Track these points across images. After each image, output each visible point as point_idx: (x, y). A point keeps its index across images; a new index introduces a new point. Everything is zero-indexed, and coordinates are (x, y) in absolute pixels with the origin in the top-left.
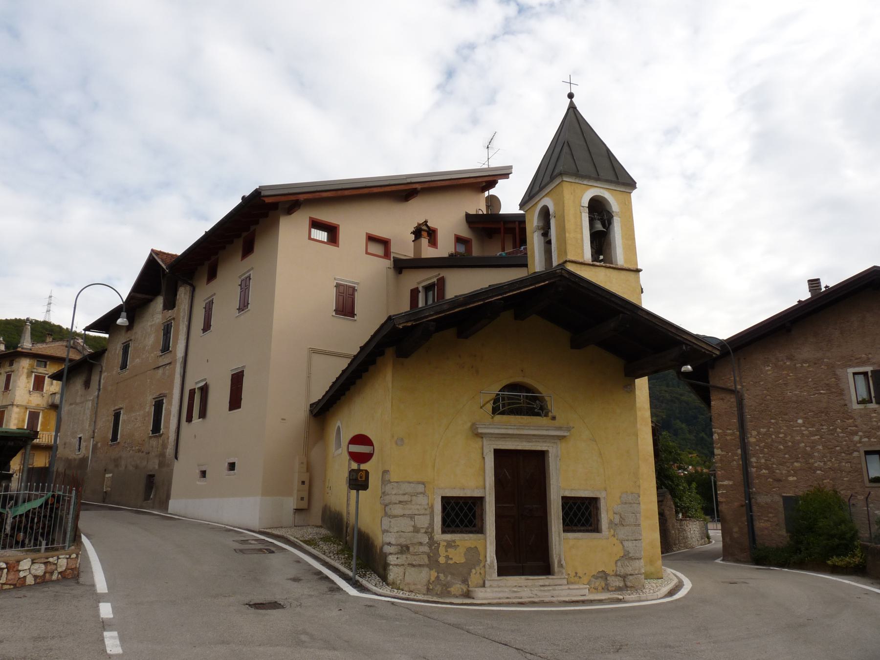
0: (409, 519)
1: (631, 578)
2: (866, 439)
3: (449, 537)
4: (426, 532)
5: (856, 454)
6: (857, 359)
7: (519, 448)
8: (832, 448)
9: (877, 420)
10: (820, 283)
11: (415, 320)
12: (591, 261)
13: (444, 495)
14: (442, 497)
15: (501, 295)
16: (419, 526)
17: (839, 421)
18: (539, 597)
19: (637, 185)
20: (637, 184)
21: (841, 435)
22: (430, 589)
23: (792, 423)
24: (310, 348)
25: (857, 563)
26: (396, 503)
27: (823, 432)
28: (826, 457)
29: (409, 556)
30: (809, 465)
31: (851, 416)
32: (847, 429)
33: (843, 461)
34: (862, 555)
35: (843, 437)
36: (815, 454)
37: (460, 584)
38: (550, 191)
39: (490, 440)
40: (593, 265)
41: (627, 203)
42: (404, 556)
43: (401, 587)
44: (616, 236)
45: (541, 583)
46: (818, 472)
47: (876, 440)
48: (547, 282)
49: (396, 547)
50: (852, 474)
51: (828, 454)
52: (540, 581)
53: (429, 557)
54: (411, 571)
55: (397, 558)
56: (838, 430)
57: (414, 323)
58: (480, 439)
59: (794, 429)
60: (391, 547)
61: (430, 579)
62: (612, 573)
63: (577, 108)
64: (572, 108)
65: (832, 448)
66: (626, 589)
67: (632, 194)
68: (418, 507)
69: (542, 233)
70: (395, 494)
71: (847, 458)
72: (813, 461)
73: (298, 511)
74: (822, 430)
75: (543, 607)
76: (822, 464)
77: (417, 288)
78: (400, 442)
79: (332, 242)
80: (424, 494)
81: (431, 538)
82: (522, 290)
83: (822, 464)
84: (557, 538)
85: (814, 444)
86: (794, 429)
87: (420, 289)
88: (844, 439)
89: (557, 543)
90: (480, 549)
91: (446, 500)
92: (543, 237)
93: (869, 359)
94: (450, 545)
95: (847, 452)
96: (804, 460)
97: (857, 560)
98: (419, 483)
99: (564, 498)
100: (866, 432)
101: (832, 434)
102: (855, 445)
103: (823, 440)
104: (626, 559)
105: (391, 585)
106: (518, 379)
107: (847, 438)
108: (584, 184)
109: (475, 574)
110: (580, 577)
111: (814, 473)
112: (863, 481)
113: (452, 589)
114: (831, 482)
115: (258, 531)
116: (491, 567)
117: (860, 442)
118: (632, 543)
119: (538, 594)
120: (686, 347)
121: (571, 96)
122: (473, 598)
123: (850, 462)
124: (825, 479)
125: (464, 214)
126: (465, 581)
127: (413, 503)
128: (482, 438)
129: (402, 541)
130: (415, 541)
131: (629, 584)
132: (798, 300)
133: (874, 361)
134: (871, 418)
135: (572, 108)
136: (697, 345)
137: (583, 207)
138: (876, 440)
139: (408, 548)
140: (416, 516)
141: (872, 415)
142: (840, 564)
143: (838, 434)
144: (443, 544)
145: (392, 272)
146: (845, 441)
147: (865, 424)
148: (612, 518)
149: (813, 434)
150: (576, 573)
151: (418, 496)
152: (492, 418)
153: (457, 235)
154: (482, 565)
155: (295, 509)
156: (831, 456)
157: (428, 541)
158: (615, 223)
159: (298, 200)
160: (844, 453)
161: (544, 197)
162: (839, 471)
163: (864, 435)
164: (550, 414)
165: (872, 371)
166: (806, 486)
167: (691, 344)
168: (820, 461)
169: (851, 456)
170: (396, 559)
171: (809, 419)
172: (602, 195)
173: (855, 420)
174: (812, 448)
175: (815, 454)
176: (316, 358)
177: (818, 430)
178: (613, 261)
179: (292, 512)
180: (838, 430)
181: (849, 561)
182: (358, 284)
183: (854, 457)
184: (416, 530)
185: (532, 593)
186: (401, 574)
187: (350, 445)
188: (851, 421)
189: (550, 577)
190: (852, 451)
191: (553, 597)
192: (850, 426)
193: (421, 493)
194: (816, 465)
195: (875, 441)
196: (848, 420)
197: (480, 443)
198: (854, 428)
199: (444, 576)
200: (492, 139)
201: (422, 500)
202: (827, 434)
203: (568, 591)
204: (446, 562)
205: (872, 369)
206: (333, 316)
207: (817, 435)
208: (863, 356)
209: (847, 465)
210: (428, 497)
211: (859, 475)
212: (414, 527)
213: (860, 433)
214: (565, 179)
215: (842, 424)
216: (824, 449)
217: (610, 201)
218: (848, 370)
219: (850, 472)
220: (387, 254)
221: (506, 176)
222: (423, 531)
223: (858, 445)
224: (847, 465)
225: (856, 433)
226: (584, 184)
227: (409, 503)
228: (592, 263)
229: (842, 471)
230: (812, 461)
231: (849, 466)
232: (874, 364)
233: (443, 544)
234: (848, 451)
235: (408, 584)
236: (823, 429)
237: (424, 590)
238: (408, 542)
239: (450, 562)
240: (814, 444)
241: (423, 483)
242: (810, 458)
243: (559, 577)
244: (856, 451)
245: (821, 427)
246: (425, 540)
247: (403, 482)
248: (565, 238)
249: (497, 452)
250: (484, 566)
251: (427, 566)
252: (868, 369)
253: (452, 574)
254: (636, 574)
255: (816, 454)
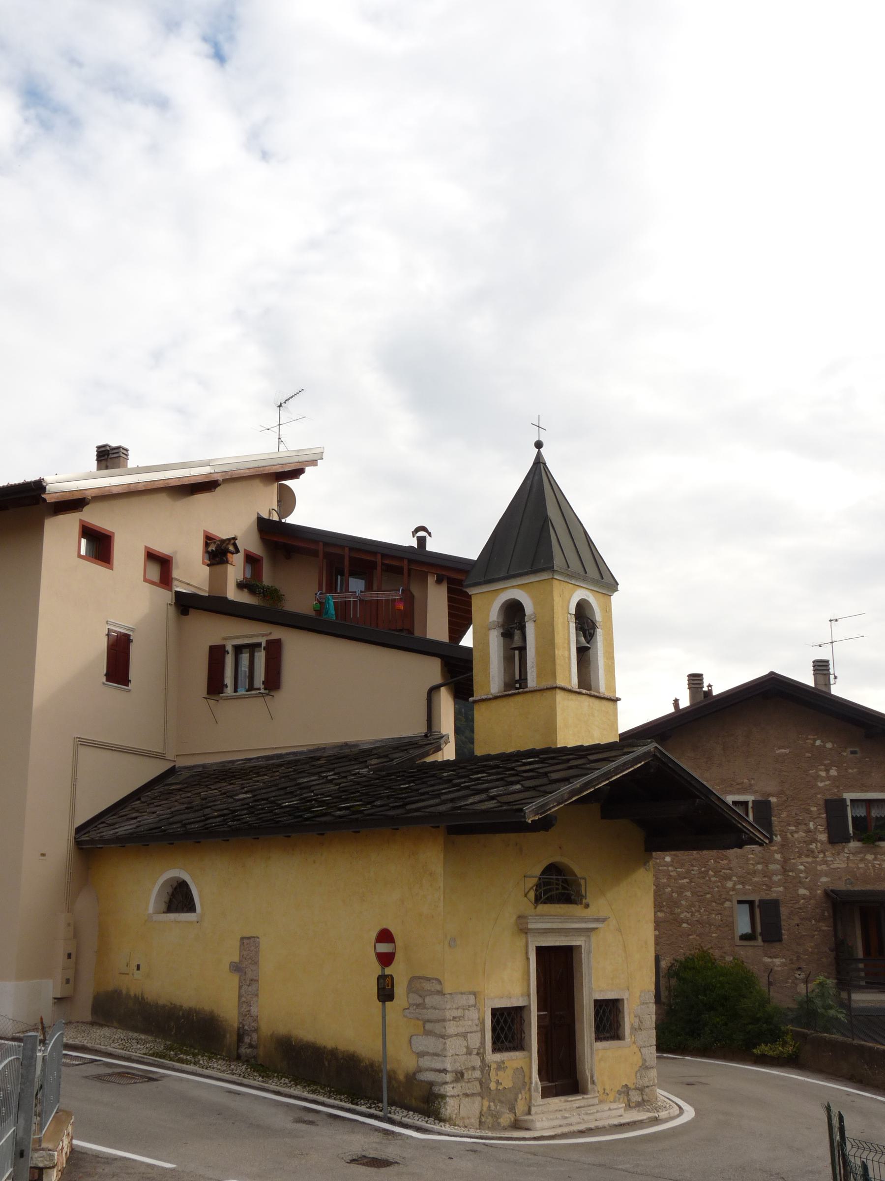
0: (463, 1039)
1: (647, 1090)
2: (739, 886)
3: (498, 1057)
4: (478, 1054)
5: (727, 904)
6: (738, 784)
7: (557, 944)
8: (702, 896)
9: (754, 862)
10: (702, 680)
11: (541, 814)
12: (577, 687)
13: (494, 1007)
14: (492, 1009)
15: (608, 779)
16: (471, 1047)
17: (712, 861)
18: (586, 1122)
19: (619, 587)
20: (619, 586)
21: (713, 879)
22: (483, 1122)
23: (658, 861)
24: (77, 738)
25: (790, 1052)
26: (450, 1020)
27: (693, 874)
28: (694, 906)
29: (463, 1084)
30: (674, 916)
31: (726, 856)
32: (721, 871)
33: (714, 912)
34: (795, 1043)
35: (715, 882)
36: (682, 902)
37: (508, 1114)
38: (527, 584)
39: (534, 936)
40: (580, 693)
41: (608, 610)
42: (459, 1085)
43: (457, 1123)
44: (599, 654)
45: (577, 1104)
46: (685, 925)
47: (750, 888)
48: (643, 763)
49: (451, 1074)
50: (721, 929)
51: (697, 903)
52: (577, 1102)
53: (481, 1084)
54: (465, 1101)
55: (453, 1088)
56: (711, 873)
57: (540, 817)
58: (523, 935)
59: (660, 868)
60: (446, 1074)
61: (482, 1110)
62: (633, 1087)
63: (547, 464)
64: (539, 464)
65: (702, 896)
66: (643, 1104)
67: (612, 597)
68: (470, 1023)
69: (502, 633)
70: (449, 1009)
71: (718, 908)
72: (679, 910)
73: (59, 1000)
74: (693, 872)
75: (612, 1134)
76: (689, 915)
77: (224, 646)
78: (452, 943)
79: (96, 558)
80: (475, 1007)
81: (483, 1061)
82: (624, 773)
83: (689, 915)
84: (589, 1050)
85: (682, 890)
86: (660, 868)
87: (229, 648)
88: (716, 884)
89: (589, 1057)
90: (526, 1070)
91: (495, 1012)
92: (502, 638)
93: (751, 785)
94: (500, 1066)
95: (718, 902)
96: (668, 910)
97: (789, 1049)
98: (470, 993)
99: (596, 1001)
100: (740, 877)
101: (704, 878)
102: (728, 893)
103: (693, 884)
104: (643, 1068)
105: (447, 1121)
106: (557, 859)
107: (719, 884)
108: (572, 584)
109: (521, 1099)
110: (608, 1094)
111: (678, 926)
112: (733, 938)
113: (501, 1120)
114: (698, 938)
115: (10, 1037)
116: (536, 1090)
117: (733, 889)
118: (649, 1050)
119: (585, 1118)
120: (745, 836)
121: (539, 445)
122: (528, 1129)
123: (721, 914)
124: (691, 935)
125: (255, 517)
126: (512, 1109)
127: (466, 1018)
128: (526, 933)
129: (458, 1067)
130: (470, 1065)
131: (645, 1097)
132: (674, 699)
133: (757, 788)
134: (748, 859)
135: (539, 464)
136: (753, 833)
137: (570, 614)
138: (750, 888)
139: (462, 1075)
140: (469, 1035)
141: (749, 856)
142: (771, 1053)
143: (710, 878)
144: (494, 1066)
145: (172, 610)
146: (718, 887)
147: (740, 867)
148: (633, 1022)
149: (681, 876)
150: (604, 1090)
151: (470, 1009)
152: (535, 908)
153: (207, 531)
154: (527, 1088)
155: (55, 998)
156: (699, 906)
157: (480, 1063)
158: (598, 636)
159: (85, 498)
160: (715, 902)
161: (513, 587)
162: (707, 925)
163: (739, 881)
164: (584, 901)
165: (753, 801)
166: (668, 942)
167: (749, 832)
168: (686, 912)
169: (722, 906)
170: (452, 1089)
171: (678, 856)
172: (587, 599)
173: (729, 861)
174: (680, 894)
175: (682, 902)
176: (83, 751)
177: (688, 872)
178: (592, 686)
179: (51, 1001)
180: (711, 873)
181: (782, 1050)
182: (132, 630)
183: (726, 907)
184: (469, 1053)
185: (580, 1118)
186: (457, 1107)
187: (377, 944)
188: (725, 862)
189: (586, 1096)
190: (724, 900)
191: (596, 1120)
192: (723, 869)
193: (472, 1006)
194: (682, 916)
195: (750, 889)
196: (722, 860)
197: (524, 940)
198: (728, 871)
199: (494, 1106)
200: (291, 398)
201: (473, 1014)
202: (698, 878)
203: (609, 1113)
204: (497, 1089)
205: (754, 799)
206: (104, 684)
207: (685, 878)
208: (746, 781)
209: (717, 917)
210: (479, 1009)
211: (730, 930)
212: (467, 1048)
213: (734, 878)
214: (555, 577)
215: (715, 865)
216: (692, 896)
217: (594, 607)
218: (727, 797)
219: (719, 926)
220: (165, 580)
221: (313, 463)
222: (475, 1052)
223: (731, 893)
224: (717, 917)
225: (728, 878)
226: (572, 584)
227: (462, 1018)
228: (578, 690)
229: (710, 925)
230: (677, 911)
231: (719, 918)
232: (756, 792)
233: (494, 1066)
234: (719, 900)
235: (463, 1118)
236: (693, 870)
237: (476, 1122)
238: (463, 1067)
239: (500, 1087)
240: (682, 890)
241: (474, 994)
242: (676, 907)
243: (592, 1096)
244: (728, 900)
245: (692, 868)
246: (478, 1063)
247: (456, 993)
248: (555, 656)
249: (540, 950)
250: (530, 1089)
251: (479, 1094)
252: (750, 798)
253: (501, 1102)
254: (652, 1086)
255: (683, 902)
